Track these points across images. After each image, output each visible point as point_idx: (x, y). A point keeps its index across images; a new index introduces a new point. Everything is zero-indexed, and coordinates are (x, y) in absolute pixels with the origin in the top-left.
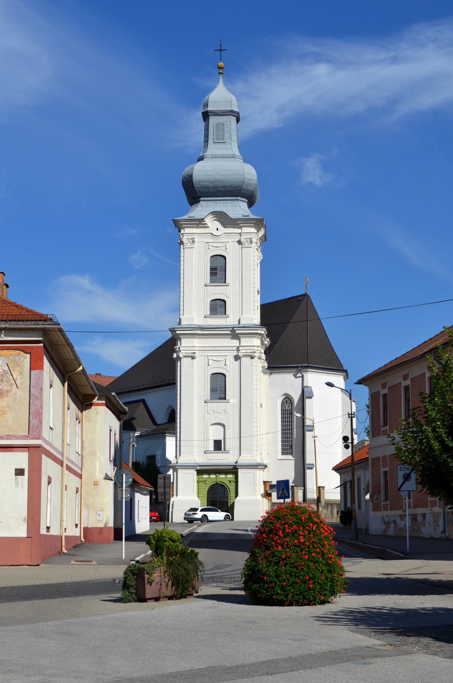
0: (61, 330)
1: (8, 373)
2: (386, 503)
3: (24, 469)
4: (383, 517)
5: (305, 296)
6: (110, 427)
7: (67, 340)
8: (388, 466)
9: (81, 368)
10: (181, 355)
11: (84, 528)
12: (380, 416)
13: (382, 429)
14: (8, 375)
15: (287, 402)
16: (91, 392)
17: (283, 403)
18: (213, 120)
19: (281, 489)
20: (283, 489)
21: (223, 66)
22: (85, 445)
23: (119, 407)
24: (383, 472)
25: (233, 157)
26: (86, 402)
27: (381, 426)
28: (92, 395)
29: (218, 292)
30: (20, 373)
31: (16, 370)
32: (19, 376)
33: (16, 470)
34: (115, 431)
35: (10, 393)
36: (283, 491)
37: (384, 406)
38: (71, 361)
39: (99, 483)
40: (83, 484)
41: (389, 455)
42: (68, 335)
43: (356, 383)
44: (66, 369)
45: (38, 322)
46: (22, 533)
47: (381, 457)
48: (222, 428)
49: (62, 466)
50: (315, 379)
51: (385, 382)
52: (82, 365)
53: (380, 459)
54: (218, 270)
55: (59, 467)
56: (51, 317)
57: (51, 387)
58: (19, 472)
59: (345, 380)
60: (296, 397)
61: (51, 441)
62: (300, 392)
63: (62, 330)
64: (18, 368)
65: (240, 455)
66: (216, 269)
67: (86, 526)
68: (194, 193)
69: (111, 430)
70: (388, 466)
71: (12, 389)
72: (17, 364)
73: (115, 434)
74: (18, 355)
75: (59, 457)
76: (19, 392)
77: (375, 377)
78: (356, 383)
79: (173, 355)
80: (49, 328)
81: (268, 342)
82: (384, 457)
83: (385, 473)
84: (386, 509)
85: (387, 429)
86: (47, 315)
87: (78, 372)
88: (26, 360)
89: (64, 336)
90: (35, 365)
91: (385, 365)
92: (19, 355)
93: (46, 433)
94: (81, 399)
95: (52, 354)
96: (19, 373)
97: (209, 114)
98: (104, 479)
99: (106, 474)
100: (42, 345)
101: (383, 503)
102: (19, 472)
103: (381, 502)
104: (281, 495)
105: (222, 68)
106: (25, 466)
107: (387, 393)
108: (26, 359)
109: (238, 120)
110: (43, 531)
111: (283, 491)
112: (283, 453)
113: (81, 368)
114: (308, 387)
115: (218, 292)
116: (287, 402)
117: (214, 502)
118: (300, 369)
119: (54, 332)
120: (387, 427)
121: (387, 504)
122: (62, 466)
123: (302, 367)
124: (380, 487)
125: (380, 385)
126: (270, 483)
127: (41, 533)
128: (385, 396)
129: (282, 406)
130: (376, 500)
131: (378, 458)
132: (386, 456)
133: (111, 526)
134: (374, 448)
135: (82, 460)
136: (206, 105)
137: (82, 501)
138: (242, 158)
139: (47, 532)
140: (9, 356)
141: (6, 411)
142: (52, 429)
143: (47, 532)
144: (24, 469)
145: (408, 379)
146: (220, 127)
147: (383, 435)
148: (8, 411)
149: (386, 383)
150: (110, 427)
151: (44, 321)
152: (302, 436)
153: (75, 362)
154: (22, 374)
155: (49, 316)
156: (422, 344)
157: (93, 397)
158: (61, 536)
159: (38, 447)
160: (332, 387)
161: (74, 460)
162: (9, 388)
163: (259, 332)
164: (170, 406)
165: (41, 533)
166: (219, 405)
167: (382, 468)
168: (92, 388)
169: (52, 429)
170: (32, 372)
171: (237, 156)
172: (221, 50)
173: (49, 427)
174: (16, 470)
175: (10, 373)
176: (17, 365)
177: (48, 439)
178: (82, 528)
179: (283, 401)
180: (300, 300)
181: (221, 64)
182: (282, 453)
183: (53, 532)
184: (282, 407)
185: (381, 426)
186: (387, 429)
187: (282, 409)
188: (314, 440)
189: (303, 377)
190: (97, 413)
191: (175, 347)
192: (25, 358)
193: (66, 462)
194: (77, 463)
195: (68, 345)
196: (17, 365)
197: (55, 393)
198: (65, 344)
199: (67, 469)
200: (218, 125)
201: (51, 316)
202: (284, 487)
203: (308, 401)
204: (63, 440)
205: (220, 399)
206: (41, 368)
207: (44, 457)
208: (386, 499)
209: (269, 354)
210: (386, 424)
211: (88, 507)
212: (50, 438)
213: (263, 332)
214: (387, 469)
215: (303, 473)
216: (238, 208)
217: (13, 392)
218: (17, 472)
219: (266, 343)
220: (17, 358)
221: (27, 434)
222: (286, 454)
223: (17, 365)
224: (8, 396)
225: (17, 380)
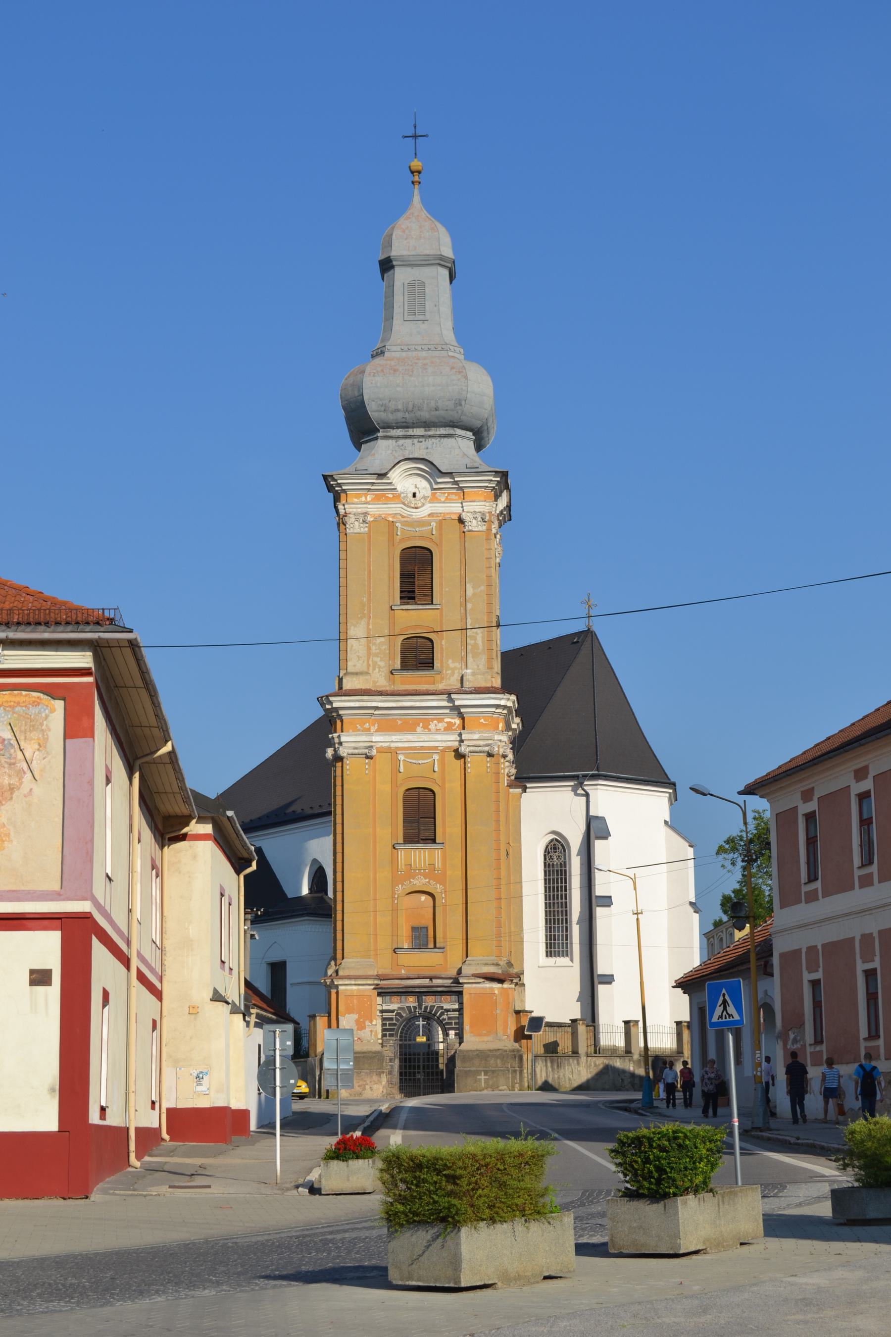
0: (133, 645)
1: (11, 745)
2: (818, 1048)
3: (50, 971)
5: (588, 635)
6: (222, 888)
7: (144, 673)
8: (821, 970)
9: (168, 748)
10: (343, 752)
11: (168, 1110)
12: (798, 862)
13: (805, 889)
14: (12, 751)
15: (555, 848)
16: (183, 810)
17: (547, 852)
18: (401, 276)
19: (720, 1001)
20: (725, 1002)
21: (420, 168)
22: (170, 925)
23: (240, 847)
24: (809, 981)
25: (443, 347)
26: (169, 833)
27: (803, 882)
28: (183, 817)
30: (39, 745)
31: (31, 739)
32: (37, 753)
33: (32, 972)
34: (230, 898)
35: (16, 794)
36: (725, 1009)
37: (808, 839)
38: (147, 730)
39: (199, 1010)
40: (164, 1013)
41: (824, 946)
42: (150, 658)
44: (138, 743)
45: (81, 627)
46: (46, 1120)
47: (820, 947)
48: (430, 898)
49: (128, 968)
50: (612, 799)
51: (810, 786)
52: (170, 739)
54: (416, 573)
55: (123, 969)
56: (112, 616)
57: (107, 784)
58: (40, 978)
59: (671, 804)
60: (575, 840)
61: (107, 908)
62: (583, 827)
63: (138, 643)
64: (34, 735)
65: (467, 956)
67: (172, 1105)
68: (362, 428)
69: (222, 895)
70: (821, 970)
71: (21, 783)
72: (35, 725)
73: (230, 904)
74: (36, 703)
75: (123, 946)
76: (37, 790)
77: (763, 786)
79: (326, 752)
80: (107, 640)
81: (518, 724)
82: (812, 950)
83: (815, 984)
85: (817, 889)
86: (103, 609)
87: (160, 756)
88: (53, 715)
89: (139, 660)
90: (76, 727)
91: (804, 753)
92: (38, 704)
93: (99, 887)
94: (160, 827)
95: (110, 709)
96: (37, 747)
97: (394, 263)
98: (211, 1000)
100: (90, 679)
102: (40, 978)
103: (804, 1046)
104: (721, 1017)
105: (419, 172)
106: (53, 962)
107: (814, 812)
108: (55, 713)
109: (452, 278)
110: (94, 1118)
111: (725, 1009)
112: (549, 954)
113: (168, 748)
114: (597, 817)
115: (415, 618)
116: (555, 848)
117: (414, 1054)
118: (581, 780)
119: (117, 651)
120: (818, 885)
121: (821, 1052)
122: (128, 968)
123: (585, 776)
125: (799, 795)
126: (530, 1015)
127: (90, 1122)
128: (810, 817)
129: (545, 856)
131: (796, 953)
134: (786, 930)
136: (389, 244)
137: (164, 1049)
138: (462, 350)
139: (101, 1119)
140: (13, 707)
141: (8, 835)
142: (110, 879)
143: (101, 1119)
144: (50, 971)
145: (867, 778)
146: (417, 290)
147: (806, 902)
148: (12, 834)
149: (812, 790)
150: (222, 888)
151: (98, 623)
152: (587, 917)
153: (156, 731)
154: (45, 747)
155: (107, 614)
156: (884, 706)
157: (186, 820)
158: (128, 1129)
159: (86, 917)
160: (705, 795)
161: (147, 957)
162: (14, 781)
163: (503, 703)
165: (90, 1122)
166: (419, 855)
167: (859, 961)
168: (186, 801)
169: (110, 879)
170: (67, 741)
171: (452, 348)
173: (104, 875)
174: (32, 972)
175: (16, 746)
176: (33, 726)
177: (102, 903)
178: (164, 1110)
179: (547, 847)
180: (577, 642)
181: (416, 164)
182: (547, 952)
183: (114, 1119)
184: (545, 859)
185: (803, 882)
186: (817, 889)
187: (545, 863)
189: (587, 795)
190: (195, 857)
191: (330, 736)
192: (53, 711)
193: (135, 963)
194: (153, 965)
195: (148, 689)
196: (33, 728)
197: (116, 800)
198: (140, 683)
199: (138, 978)
200: (411, 285)
201: (112, 612)
202: (727, 997)
203: (598, 845)
204: (130, 911)
206: (90, 733)
207: (95, 941)
208: (818, 1041)
209: (518, 752)
210: (812, 877)
211: (176, 1063)
212: (107, 902)
213: (510, 704)
214: (818, 975)
215: (590, 994)
216: (457, 450)
217: (25, 789)
218: (34, 976)
219: (514, 726)
220: (33, 711)
221: (56, 887)
222: (551, 956)
223: (33, 726)
224: (11, 798)
225: (34, 762)
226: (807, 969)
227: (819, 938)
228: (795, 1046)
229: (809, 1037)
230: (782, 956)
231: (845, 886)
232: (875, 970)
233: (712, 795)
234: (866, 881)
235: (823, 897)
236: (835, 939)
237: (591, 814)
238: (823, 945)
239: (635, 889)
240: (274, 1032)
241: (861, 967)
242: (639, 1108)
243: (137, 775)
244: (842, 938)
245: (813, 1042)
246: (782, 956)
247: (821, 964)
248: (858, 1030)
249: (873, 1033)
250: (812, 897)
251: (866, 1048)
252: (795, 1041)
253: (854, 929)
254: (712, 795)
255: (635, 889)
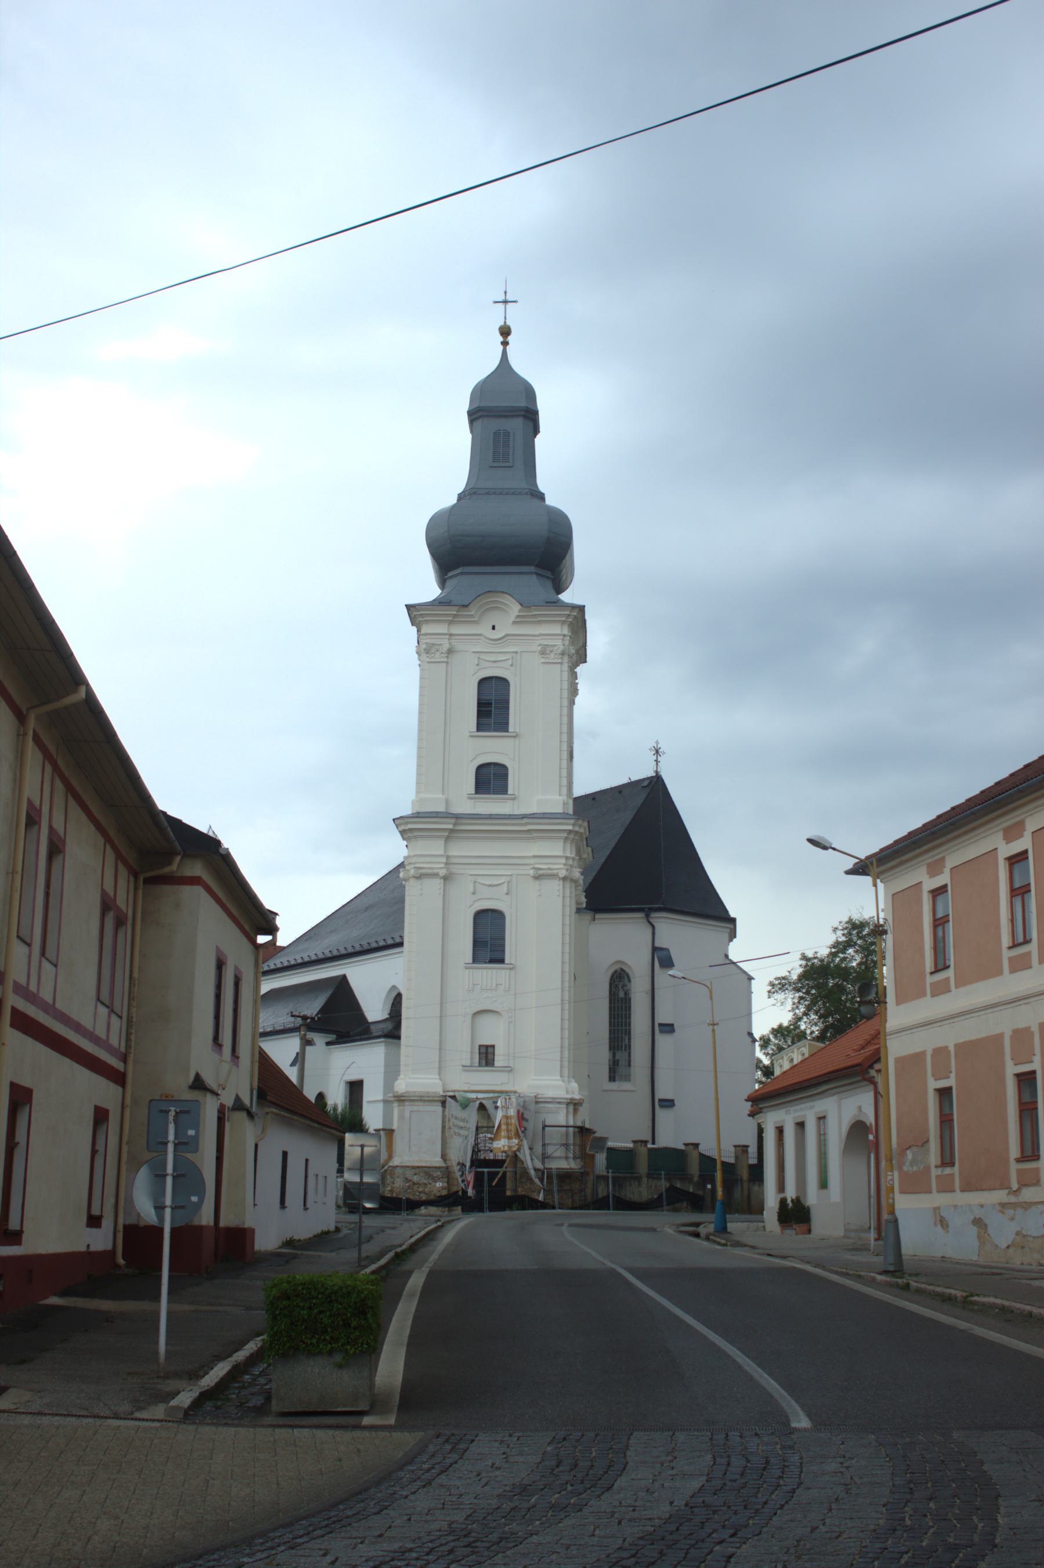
2: (948, 1171)
4: (936, 1210)
8: (953, 1075)
11: (125, 1227)
29: (493, 748)
37: (935, 920)
43: (848, 872)
47: (952, 1049)
53: (925, 1060)
66: (490, 704)
70: (953, 1075)
78: (848, 872)
83: (944, 1094)
84: (946, 1187)
99: (237, 1096)
101: (935, 1172)
103: (927, 1169)
115: (493, 748)
120: (950, 973)
121: (952, 1175)
124: (927, 1130)
130: (911, 1165)
132: (1027, 1030)
133: (204, 1223)
135: (128, 1034)
145: (1022, 836)
147: (933, 995)
160: (825, 848)
164: (394, 987)
166: (489, 974)
172: (505, 302)
178: (120, 1227)
186: (947, 979)
188: (713, 1030)
205: (492, 961)
219: (585, 856)
226: (1033, 1033)
227: (950, 1037)
228: (915, 1168)
229: (933, 1155)
230: (898, 1060)
231: (990, 970)
232: (1034, 1072)
233: (834, 849)
234: (1020, 965)
235: (956, 987)
236: (973, 1038)
237: (656, 945)
238: (956, 1046)
239: (711, 998)
240: (167, 1112)
241: (1011, 1070)
242: (710, 1234)
243: (174, 868)
244: (983, 1035)
245: (939, 1163)
246: (898, 1060)
247: (953, 1069)
248: (1007, 1149)
249: (1029, 1152)
250: (941, 989)
251: (1019, 1171)
252: (913, 1162)
253: (1003, 1024)
254: (834, 849)
255: (711, 998)
